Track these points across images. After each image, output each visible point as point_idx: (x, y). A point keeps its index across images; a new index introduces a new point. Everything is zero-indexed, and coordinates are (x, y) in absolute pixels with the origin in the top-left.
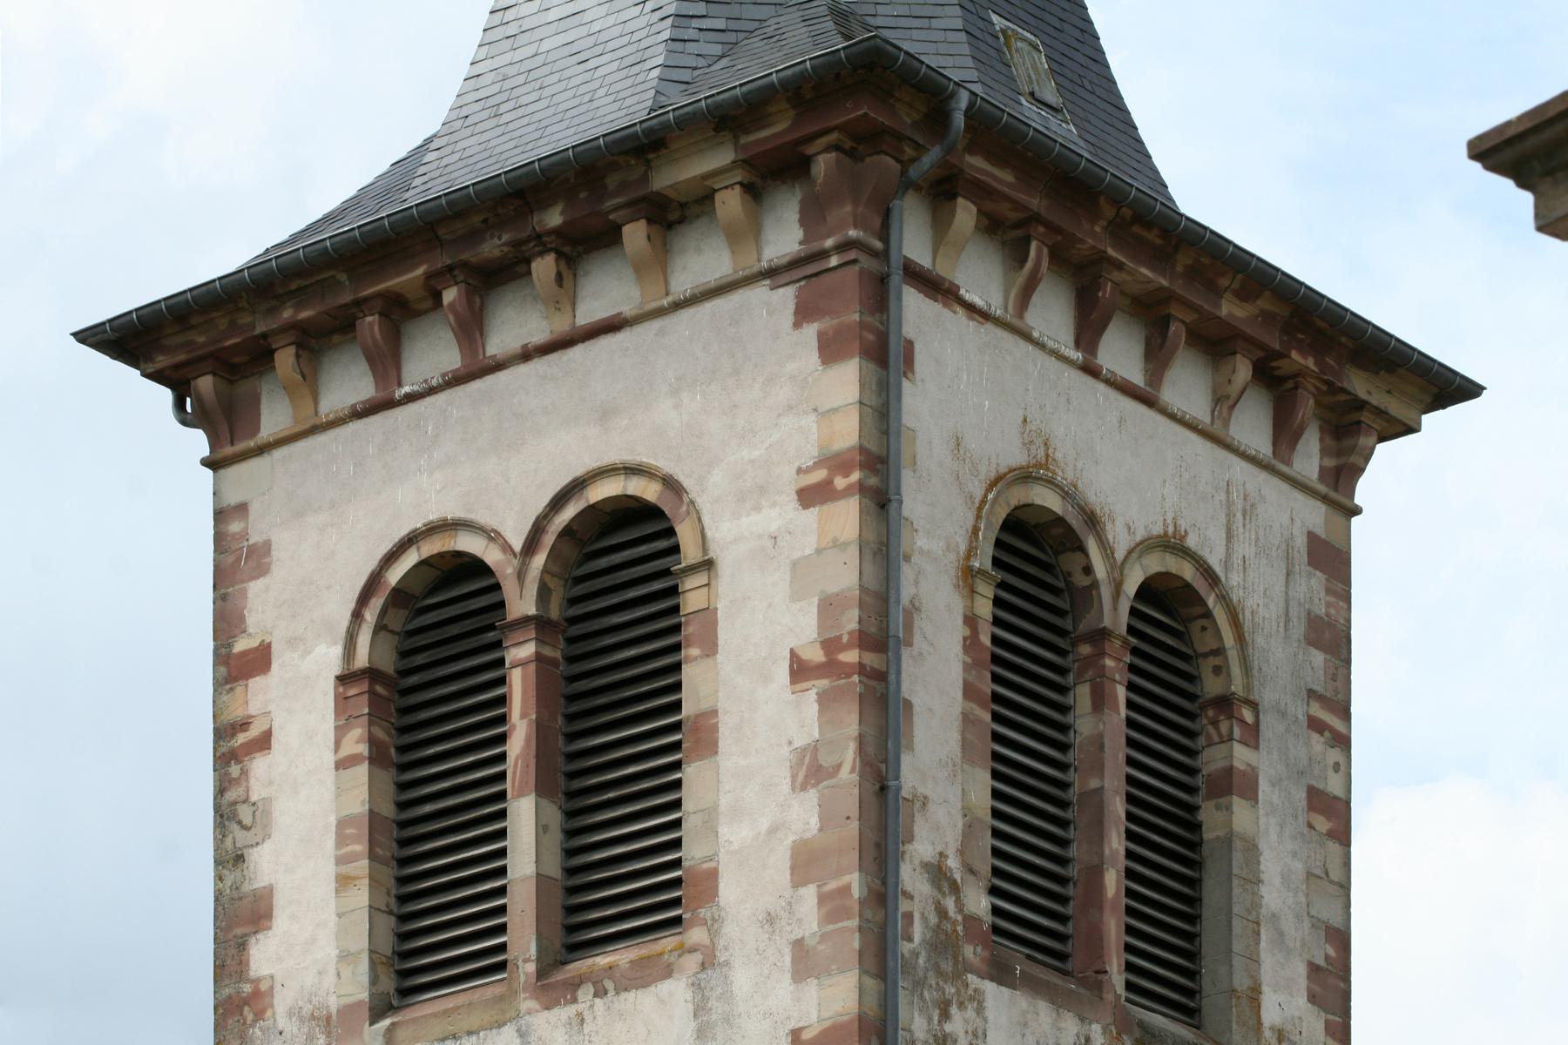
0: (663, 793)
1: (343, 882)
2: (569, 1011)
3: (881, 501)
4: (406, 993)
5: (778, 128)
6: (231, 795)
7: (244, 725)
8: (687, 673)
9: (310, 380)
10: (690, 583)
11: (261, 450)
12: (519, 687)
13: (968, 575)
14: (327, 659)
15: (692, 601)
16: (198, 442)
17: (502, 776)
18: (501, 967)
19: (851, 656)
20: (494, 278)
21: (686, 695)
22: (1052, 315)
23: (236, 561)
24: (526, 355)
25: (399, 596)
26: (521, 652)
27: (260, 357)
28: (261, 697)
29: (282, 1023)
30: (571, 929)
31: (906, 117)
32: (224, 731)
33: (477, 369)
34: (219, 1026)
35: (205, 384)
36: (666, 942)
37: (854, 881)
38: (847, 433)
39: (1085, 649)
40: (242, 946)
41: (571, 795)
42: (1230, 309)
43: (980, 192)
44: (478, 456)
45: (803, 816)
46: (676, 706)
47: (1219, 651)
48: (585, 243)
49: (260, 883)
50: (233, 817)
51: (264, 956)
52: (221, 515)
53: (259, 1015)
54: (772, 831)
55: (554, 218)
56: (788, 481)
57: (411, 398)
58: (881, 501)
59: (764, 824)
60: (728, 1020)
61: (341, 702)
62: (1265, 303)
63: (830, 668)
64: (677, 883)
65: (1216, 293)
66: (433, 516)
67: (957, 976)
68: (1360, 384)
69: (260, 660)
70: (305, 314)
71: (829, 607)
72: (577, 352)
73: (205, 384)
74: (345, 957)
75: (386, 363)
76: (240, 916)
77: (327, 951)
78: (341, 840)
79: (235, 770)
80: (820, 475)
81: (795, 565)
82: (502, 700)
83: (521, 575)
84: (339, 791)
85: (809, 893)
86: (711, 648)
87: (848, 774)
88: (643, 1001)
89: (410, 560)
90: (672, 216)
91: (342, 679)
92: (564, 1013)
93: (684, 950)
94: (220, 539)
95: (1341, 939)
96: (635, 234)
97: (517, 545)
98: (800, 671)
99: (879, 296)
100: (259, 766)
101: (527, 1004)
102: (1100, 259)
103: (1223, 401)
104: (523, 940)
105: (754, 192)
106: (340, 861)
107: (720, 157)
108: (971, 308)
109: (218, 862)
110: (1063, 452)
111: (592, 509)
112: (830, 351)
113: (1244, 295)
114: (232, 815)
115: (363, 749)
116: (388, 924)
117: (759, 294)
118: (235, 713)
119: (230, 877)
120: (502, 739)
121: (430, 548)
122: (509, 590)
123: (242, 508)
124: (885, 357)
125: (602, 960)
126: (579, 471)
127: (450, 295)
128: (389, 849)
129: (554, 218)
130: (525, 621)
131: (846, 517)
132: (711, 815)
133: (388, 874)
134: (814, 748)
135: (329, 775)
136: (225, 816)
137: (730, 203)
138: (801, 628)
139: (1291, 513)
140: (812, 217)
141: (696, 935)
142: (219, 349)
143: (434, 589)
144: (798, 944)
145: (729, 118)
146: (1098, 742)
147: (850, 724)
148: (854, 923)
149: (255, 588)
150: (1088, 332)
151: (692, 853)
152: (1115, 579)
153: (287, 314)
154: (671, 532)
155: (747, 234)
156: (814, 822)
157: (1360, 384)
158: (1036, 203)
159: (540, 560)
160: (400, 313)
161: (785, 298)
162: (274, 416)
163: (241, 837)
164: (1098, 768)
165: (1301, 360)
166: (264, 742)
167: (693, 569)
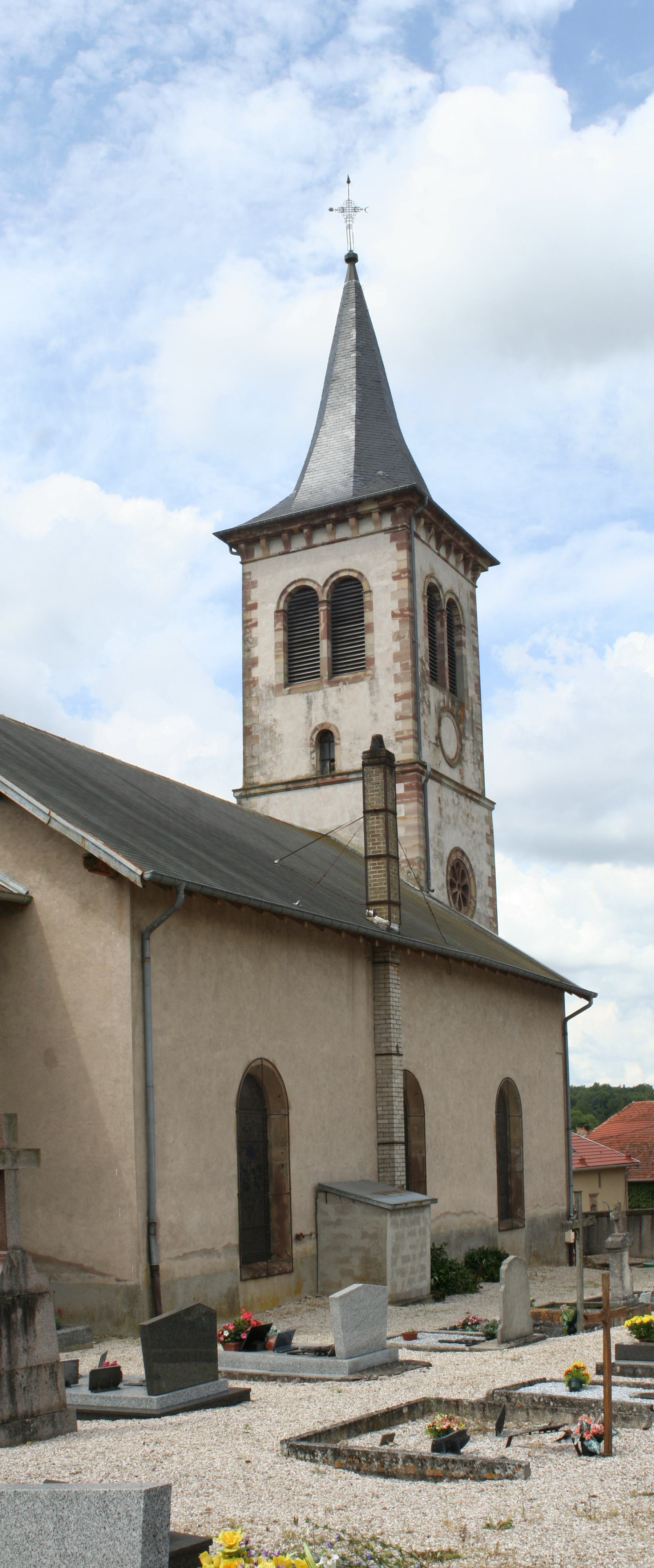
0: (359, 641)
1: (277, 657)
2: (337, 688)
3: (412, 580)
4: (290, 682)
5: (389, 501)
6: (247, 636)
7: (250, 620)
8: (365, 614)
9: (268, 547)
10: (366, 595)
11: (255, 561)
12: (322, 616)
13: (424, 596)
14: (273, 607)
15: (366, 598)
16: (238, 558)
17: (318, 634)
18: (319, 676)
19: (407, 613)
20: (314, 528)
21: (365, 619)
22: (433, 543)
23: (248, 585)
24: (323, 544)
25: (290, 594)
26: (323, 608)
27: (257, 541)
28: (254, 614)
29: (261, 687)
30: (334, 669)
31: (415, 500)
32: (245, 622)
33: (310, 546)
34: (244, 688)
35: (242, 546)
36: (360, 673)
37: (410, 662)
38: (404, 565)
39: (439, 614)
40: (250, 670)
41: (333, 640)
42: (461, 544)
43: (425, 517)
44: (316, 565)
45: (396, 647)
46: (363, 621)
47: (458, 615)
48: (337, 522)
49: (255, 656)
50: (248, 641)
51: (255, 672)
52: (244, 574)
53: (255, 686)
54: (388, 650)
55: (333, 516)
56: (390, 575)
57: (294, 552)
58: (412, 580)
59: (386, 648)
60: (378, 691)
61: (276, 617)
62: (467, 543)
63: (402, 615)
64: (364, 660)
65: (459, 540)
66: (300, 577)
67: (425, 683)
68: (480, 561)
69: (255, 606)
70: (270, 532)
71: (401, 602)
72: (336, 544)
73: (242, 546)
74: (277, 673)
75: (287, 544)
76: (249, 663)
77: (273, 672)
78: (276, 647)
79: (248, 630)
80: (398, 574)
81: (392, 593)
82: (318, 618)
83: (323, 591)
84: (275, 637)
85: (398, 664)
86: (371, 609)
87: (407, 638)
88: (356, 687)
89: (294, 586)
90: (360, 517)
91: (277, 612)
92: (335, 688)
93: (366, 675)
94: (244, 579)
95: (478, 678)
96: (352, 521)
97: (322, 584)
98: (394, 615)
99: (409, 538)
100: (254, 630)
101: (325, 686)
102: (443, 532)
103: (457, 562)
104: (324, 671)
105: (380, 513)
106: (276, 652)
107: (374, 506)
108: (422, 541)
109: (244, 651)
110: (436, 572)
111: (340, 578)
112: (399, 547)
113: (464, 541)
114: (247, 642)
115: (282, 627)
116: (287, 666)
117: (382, 535)
118: (248, 617)
119: (247, 654)
120: (318, 626)
121: (299, 584)
122: (319, 594)
123: (250, 573)
124: (411, 550)
125: (344, 676)
126: (337, 570)
127: (305, 531)
128: (287, 650)
129: (333, 516)
130: (323, 601)
131: (405, 583)
132: (372, 646)
133: (287, 655)
134: (398, 632)
135: (273, 633)
136: (245, 640)
137: (376, 516)
138: (395, 606)
139: (467, 586)
140: (394, 519)
141: (369, 672)
142: (243, 540)
143: (297, 593)
144: (396, 675)
145: (377, 499)
146: (443, 634)
147: (407, 627)
148: (410, 671)
149: (253, 591)
150: (438, 548)
151: (368, 653)
152: (445, 598)
153: (265, 532)
154: (360, 583)
155: (378, 522)
156: (399, 648)
157: (480, 561)
158: (434, 520)
159: (327, 588)
160: (292, 533)
161: (388, 536)
162: (258, 553)
163: (250, 645)
164: (443, 639)
165: (472, 555)
166: (256, 624)
167: (366, 592)
